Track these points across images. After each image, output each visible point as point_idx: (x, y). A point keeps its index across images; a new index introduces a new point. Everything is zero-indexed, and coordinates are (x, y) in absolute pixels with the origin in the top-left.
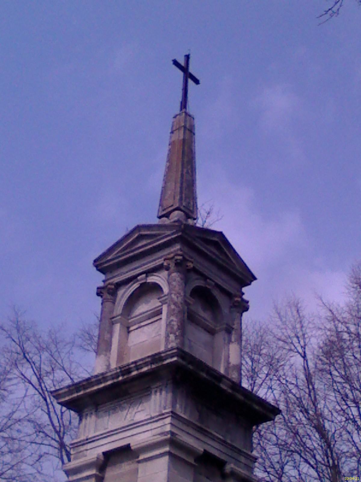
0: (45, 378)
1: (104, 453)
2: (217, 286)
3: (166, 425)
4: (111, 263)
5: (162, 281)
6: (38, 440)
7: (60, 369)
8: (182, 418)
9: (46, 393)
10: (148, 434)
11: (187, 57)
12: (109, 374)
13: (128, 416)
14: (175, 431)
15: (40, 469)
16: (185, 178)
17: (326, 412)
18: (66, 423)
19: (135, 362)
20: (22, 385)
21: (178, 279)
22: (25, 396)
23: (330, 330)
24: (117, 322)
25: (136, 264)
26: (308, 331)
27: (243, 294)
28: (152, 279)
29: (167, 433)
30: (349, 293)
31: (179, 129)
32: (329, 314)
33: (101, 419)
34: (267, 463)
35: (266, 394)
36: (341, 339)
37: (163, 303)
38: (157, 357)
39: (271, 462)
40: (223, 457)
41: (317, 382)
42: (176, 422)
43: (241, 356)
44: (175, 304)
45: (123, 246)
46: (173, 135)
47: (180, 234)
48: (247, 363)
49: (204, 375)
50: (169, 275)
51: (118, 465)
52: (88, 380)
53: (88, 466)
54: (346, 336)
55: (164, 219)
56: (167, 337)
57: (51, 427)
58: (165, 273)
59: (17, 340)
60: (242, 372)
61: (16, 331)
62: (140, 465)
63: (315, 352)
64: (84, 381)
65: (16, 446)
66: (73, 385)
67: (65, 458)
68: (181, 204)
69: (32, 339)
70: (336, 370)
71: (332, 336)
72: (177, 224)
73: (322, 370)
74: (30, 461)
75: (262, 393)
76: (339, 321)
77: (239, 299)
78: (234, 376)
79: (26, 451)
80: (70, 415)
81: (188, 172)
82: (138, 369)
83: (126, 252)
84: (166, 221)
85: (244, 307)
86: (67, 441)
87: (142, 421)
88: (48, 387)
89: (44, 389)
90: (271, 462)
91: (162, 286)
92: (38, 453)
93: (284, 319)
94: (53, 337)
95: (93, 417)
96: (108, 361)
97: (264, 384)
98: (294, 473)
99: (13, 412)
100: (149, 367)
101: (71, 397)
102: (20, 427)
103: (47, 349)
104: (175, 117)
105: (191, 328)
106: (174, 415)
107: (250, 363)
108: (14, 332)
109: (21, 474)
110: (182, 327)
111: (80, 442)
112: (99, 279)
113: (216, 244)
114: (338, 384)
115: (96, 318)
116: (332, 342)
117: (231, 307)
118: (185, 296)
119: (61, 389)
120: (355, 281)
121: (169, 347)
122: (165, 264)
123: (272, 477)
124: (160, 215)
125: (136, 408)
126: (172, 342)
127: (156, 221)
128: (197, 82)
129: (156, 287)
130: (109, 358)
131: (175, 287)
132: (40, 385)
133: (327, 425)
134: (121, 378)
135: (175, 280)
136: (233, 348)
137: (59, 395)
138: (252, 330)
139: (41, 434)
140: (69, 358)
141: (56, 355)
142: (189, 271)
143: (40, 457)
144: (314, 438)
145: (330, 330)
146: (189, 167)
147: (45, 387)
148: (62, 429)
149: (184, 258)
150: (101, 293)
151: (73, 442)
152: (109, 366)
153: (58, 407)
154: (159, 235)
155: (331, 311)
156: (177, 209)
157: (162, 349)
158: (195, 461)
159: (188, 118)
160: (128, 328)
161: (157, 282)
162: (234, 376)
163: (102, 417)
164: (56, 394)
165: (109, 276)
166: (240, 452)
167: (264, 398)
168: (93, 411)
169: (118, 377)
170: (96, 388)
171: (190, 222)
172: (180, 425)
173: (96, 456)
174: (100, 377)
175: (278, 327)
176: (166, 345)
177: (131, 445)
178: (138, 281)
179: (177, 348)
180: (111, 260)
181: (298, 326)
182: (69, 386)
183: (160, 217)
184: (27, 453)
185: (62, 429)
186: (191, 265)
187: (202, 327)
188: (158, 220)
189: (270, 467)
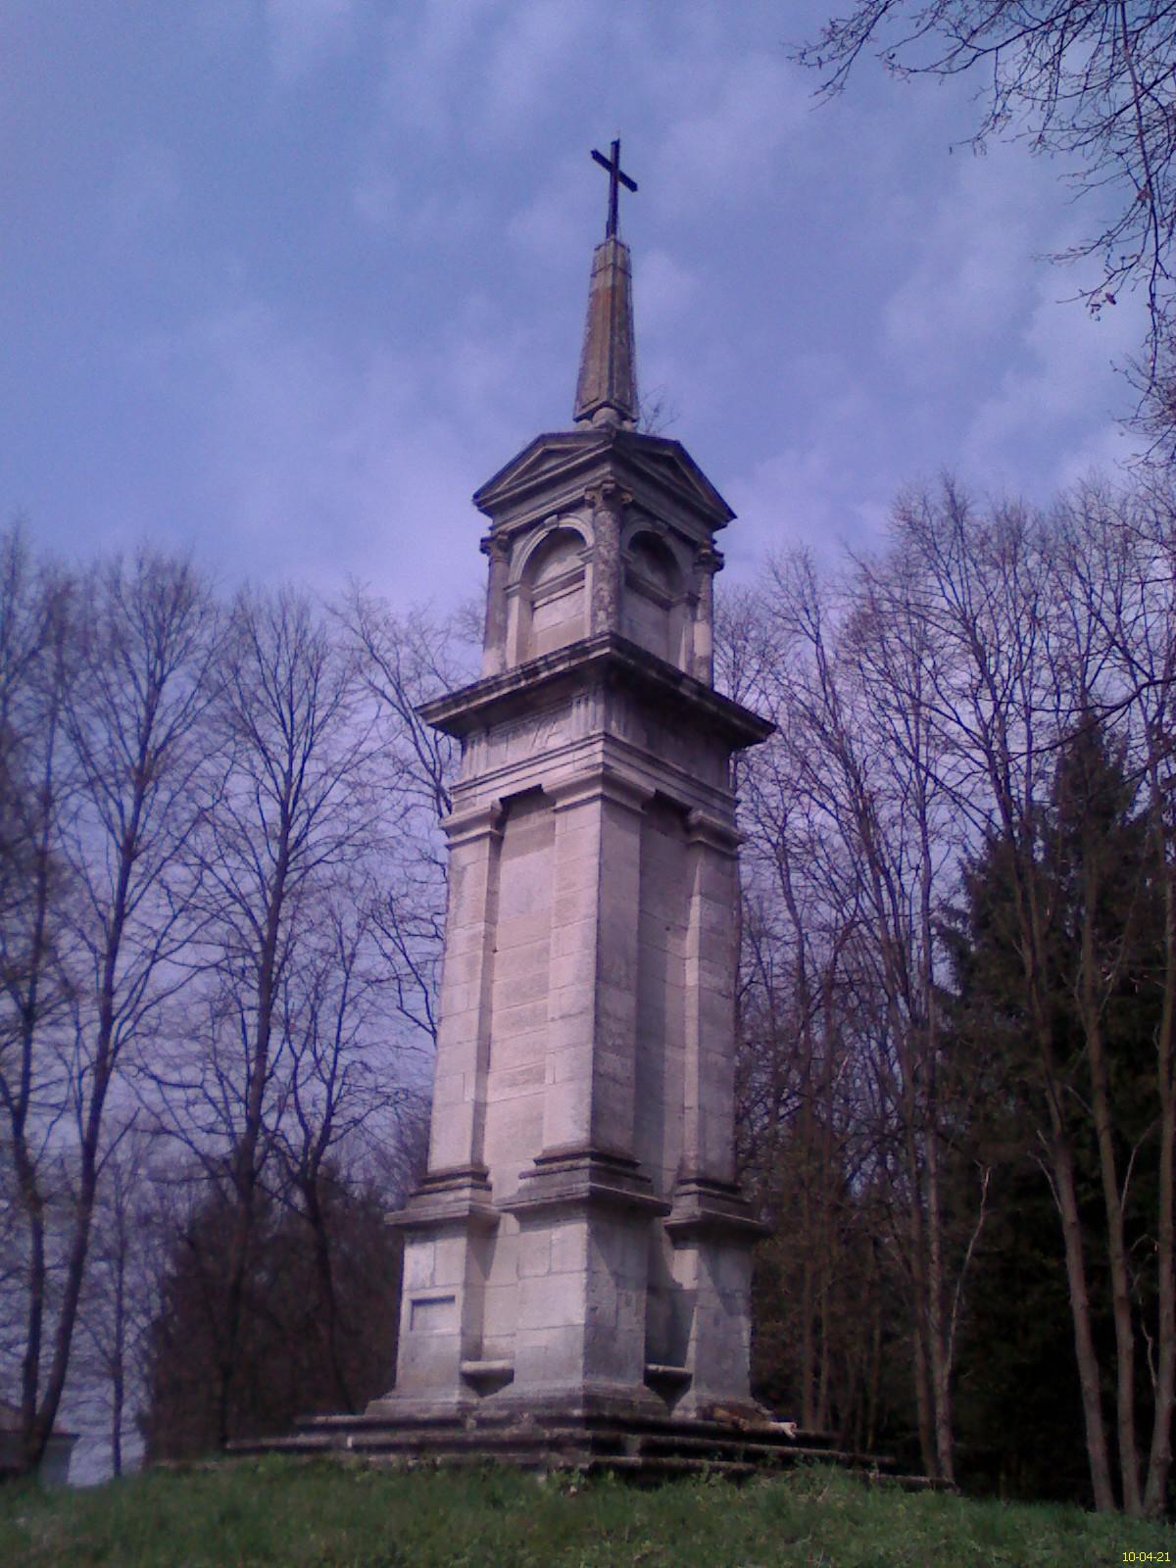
0: (406, 688)
1: (502, 800)
2: (672, 530)
3: (597, 753)
4: (502, 498)
5: (584, 526)
6: (402, 785)
7: (429, 673)
8: (621, 742)
9: (410, 712)
10: (569, 769)
11: (616, 145)
12: (504, 678)
13: (538, 741)
14: (611, 763)
15: (406, 829)
16: (616, 352)
17: (855, 729)
18: (445, 758)
19: (545, 657)
20: (372, 700)
21: (609, 522)
22: (377, 717)
23: (860, 597)
24: (514, 594)
25: (543, 499)
26: (823, 599)
27: (715, 542)
28: (569, 522)
29: (598, 765)
30: (892, 536)
31: (604, 269)
32: (860, 571)
33: (496, 748)
34: (762, 810)
35: (757, 701)
36: (877, 611)
37: (586, 561)
38: (578, 648)
39: (768, 808)
40: (688, 802)
41: (840, 680)
42: (611, 749)
43: (714, 640)
44: (606, 562)
45: (528, 462)
46: (596, 280)
47: (610, 446)
48: (725, 654)
49: (654, 675)
50: (595, 514)
51: (525, 818)
52: (472, 687)
53: (478, 820)
54: (886, 606)
55: (584, 422)
56: (594, 615)
57: (420, 764)
58: (587, 513)
59: (358, 629)
60: (716, 666)
61: (356, 614)
62: (558, 817)
63: (837, 633)
64: (465, 689)
65: (368, 795)
66: (449, 696)
67: (445, 810)
68: (612, 396)
69: (382, 627)
70: (871, 661)
71: (864, 606)
72: (604, 430)
73: (845, 662)
74: (391, 816)
75: (750, 701)
76: (876, 582)
77: (708, 551)
78: (702, 674)
79: (385, 801)
80: (449, 743)
81: (621, 342)
82: (549, 669)
83: (526, 478)
84: (587, 426)
85: (717, 564)
86: (446, 783)
87: (557, 750)
88: (412, 702)
89: (407, 705)
90: (768, 808)
91: (584, 534)
92: (403, 803)
93: (784, 582)
94: (416, 623)
95: (484, 745)
96: (503, 655)
97: (753, 687)
98: (802, 823)
99: (360, 743)
100: (566, 665)
101: (446, 715)
102: (372, 766)
103: (409, 642)
104: (598, 249)
105: (632, 600)
106: (608, 738)
107: (731, 653)
108: (354, 615)
109: (378, 837)
110: (618, 599)
111: (465, 783)
112: (482, 525)
113: (670, 462)
114: (873, 684)
115: (480, 588)
116: (865, 616)
117: (695, 564)
118: (620, 548)
119: (431, 703)
120: (902, 514)
121: (598, 631)
122: (587, 498)
123: (768, 830)
124: (578, 414)
125: (548, 729)
126: (602, 623)
127: (569, 426)
128: (633, 186)
129: (575, 536)
130: (504, 651)
131: (604, 534)
132: (400, 698)
133: (856, 747)
134: (523, 683)
135: (603, 524)
136: (700, 630)
137: (430, 712)
138: (732, 599)
139: (407, 776)
140: (442, 654)
141: (422, 651)
142: (626, 507)
143: (407, 809)
144: (835, 769)
145: (860, 597)
146: (623, 332)
147: (408, 702)
148: (438, 766)
149: (617, 486)
150: (487, 547)
151: (455, 784)
152: (504, 665)
153: (430, 732)
154: (578, 449)
155: (863, 566)
156: (606, 405)
157: (587, 635)
158: (643, 808)
159: (620, 249)
160: (533, 603)
161: (576, 527)
162: (701, 675)
163: (496, 744)
164: (424, 711)
165: (500, 520)
166: (711, 792)
167: (752, 709)
168: (483, 735)
169: (520, 681)
170: (485, 699)
171: (627, 426)
172: (618, 753)
173: (490, 804)
174: (491, 683)
175: (775, 594)
176: (592, 628)
177: (543, 786)
178: (544, 527)
179: (611, 633)
180: (498, 495)
181: (807, 591)
182: (443, 699)
183: (578, 420)
184: (386, 805)
185: (438, 766)
186: (629, 498)
187: (650, 599)
188: (574, 423)
189: (765, 815)
